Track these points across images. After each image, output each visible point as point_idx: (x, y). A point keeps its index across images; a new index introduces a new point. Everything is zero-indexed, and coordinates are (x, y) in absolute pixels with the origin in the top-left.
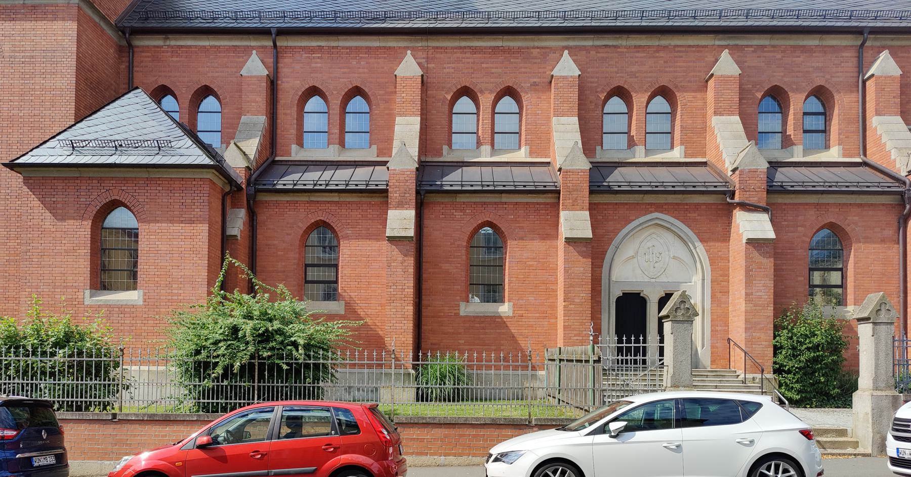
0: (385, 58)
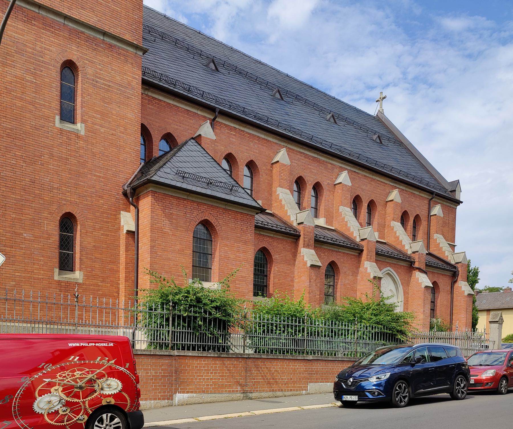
0: (266, 147)
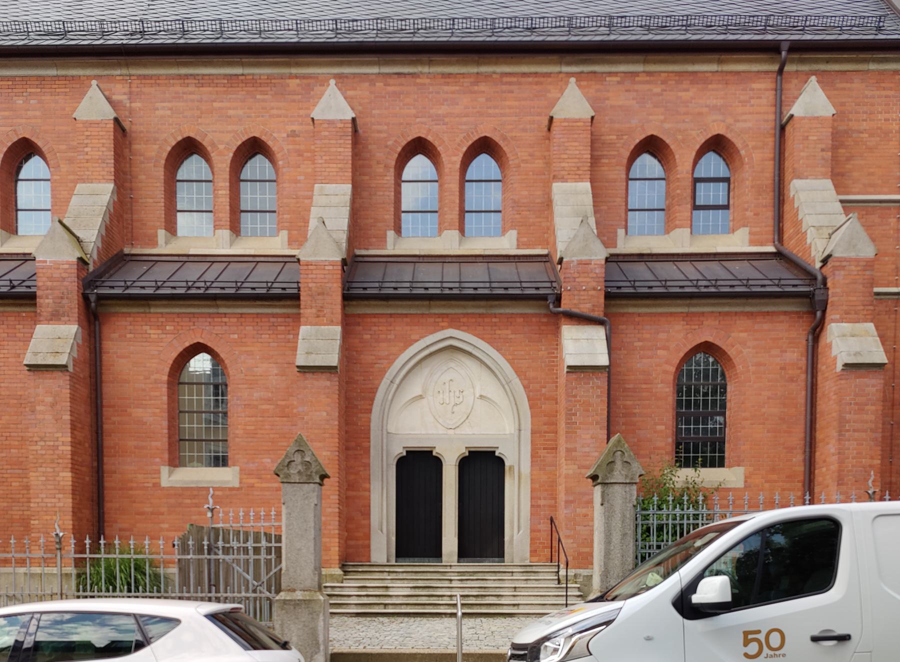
0: (66, 94)
